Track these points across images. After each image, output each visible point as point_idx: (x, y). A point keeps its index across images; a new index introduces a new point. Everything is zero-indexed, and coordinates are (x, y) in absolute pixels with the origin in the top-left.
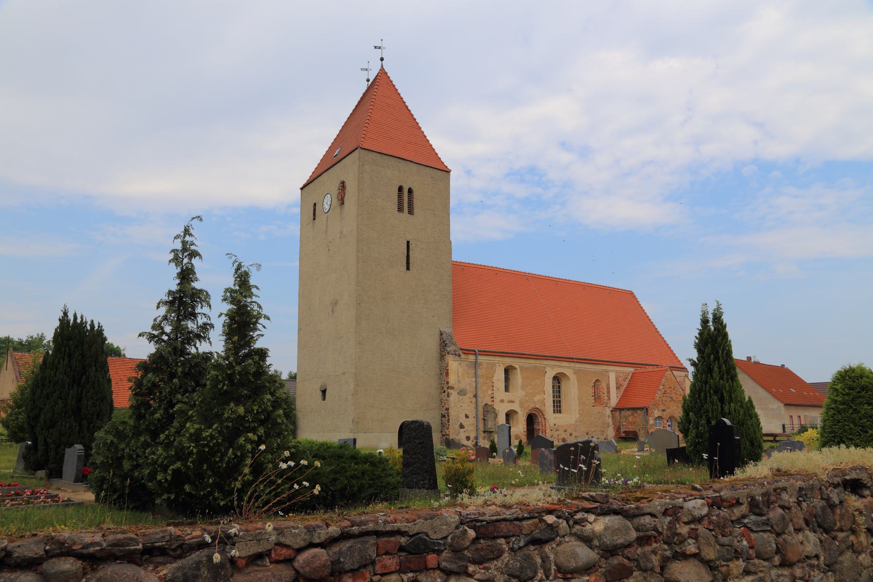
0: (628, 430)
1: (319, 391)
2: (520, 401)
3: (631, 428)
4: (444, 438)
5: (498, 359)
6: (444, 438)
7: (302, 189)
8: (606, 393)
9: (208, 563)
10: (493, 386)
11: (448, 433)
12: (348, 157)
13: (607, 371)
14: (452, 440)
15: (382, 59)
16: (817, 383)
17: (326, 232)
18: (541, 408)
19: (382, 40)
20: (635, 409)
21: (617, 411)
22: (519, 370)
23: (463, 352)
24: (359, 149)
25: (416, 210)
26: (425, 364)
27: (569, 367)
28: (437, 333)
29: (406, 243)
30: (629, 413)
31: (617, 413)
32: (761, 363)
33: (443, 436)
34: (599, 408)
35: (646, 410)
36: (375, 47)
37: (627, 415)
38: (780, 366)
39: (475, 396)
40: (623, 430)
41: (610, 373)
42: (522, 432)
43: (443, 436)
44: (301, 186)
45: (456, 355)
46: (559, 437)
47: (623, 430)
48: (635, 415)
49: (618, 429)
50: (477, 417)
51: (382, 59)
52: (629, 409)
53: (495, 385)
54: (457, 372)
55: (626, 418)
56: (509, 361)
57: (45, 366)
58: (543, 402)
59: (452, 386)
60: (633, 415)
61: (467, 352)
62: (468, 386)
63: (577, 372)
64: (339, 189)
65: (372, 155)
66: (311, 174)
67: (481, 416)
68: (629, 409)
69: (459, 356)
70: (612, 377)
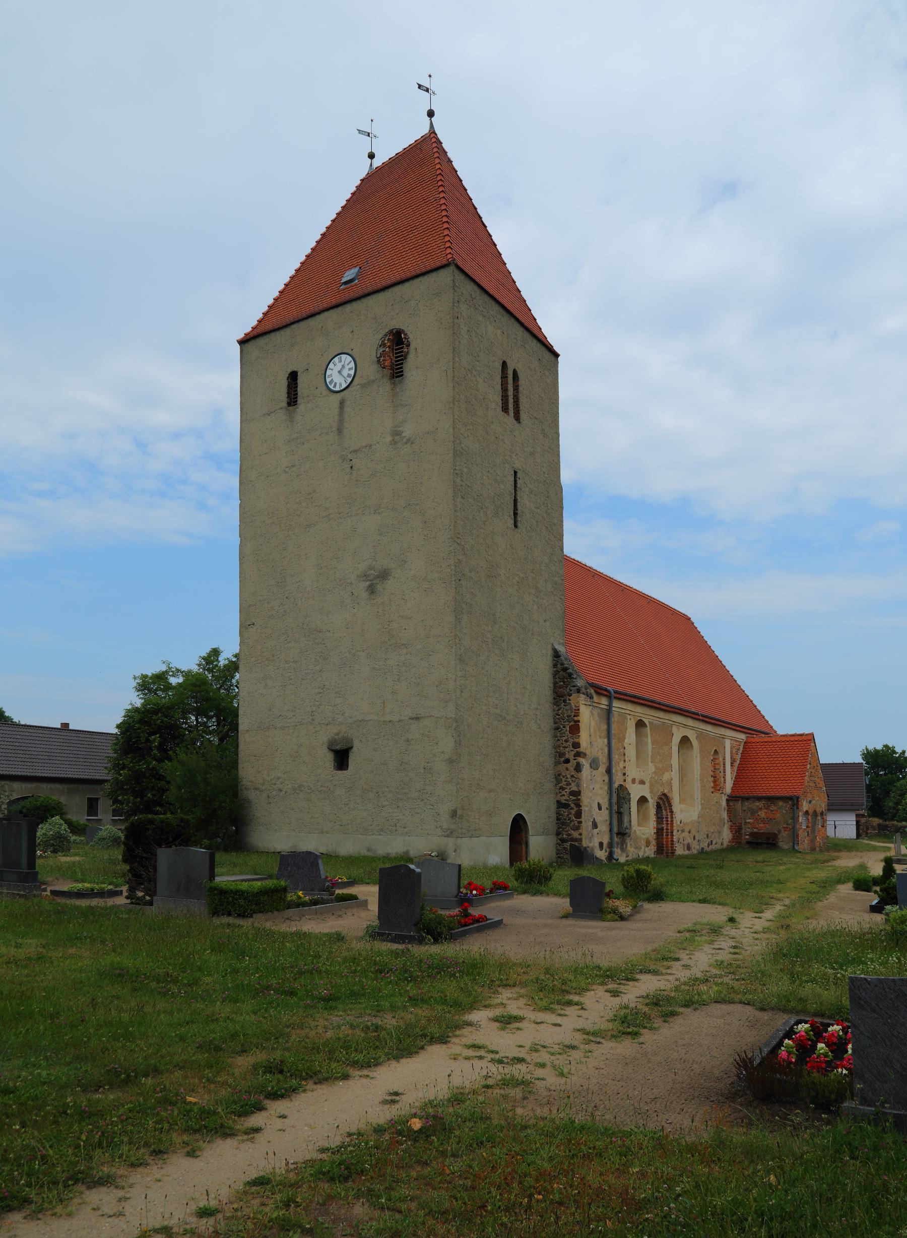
0: (755, 830)
1: (326, 750)
2: (650, 782)
3: (762, 828)
4: (567, 845)
5: (630, 707)
6: (567, 845)
7: (242, 342)
8: (722, 772)
9: (332, 1175)
10: (624, 755)
11: (575, 834)
12: (416, 282)
13: (723, 737)
14: (585, 848)
15: (431, 114)
16: (836, 764)
17: (340, 431)
18: (668, 795)
19: (430, 76)
20: (772, 799)
21: (738, 801)
22: (648, 728)
23: (596, 692)
24: (452, 267)
25: (523, 416)
26: (537, 709)
27: (693, 728)
28: (550, 653)
29: (513, 473)
30: (760, 804)
31: (739, 805)
32: (22, 723)
33: (563, 841)
34: (717, 795)
35: (794, 801)
36: (420, 86)
37: (755, 808)
38: (59, 727)
39: (609, 771)
40: (746, 830)
41: (726, 740)
42: (653, 833)
43: (563, 841)
44: (241, 336)
45: (588, 696)
46: (685, 842)
47: (746, 830)
48: (773, 808)
49: (737, 831)
50: (610, 808)
51: (431, 114)
52: (759, 799)
53: (626, 751)
54: (588, 727)
55: (753, 812)
56: (641, 712)
57: (458, 617)
58: (670, 783)
59: (584, 751)
60: (767, 808)
61: (600, 691)
62: (600, 752)
63: (701, 736)
64: (383, 345)
65: (471, 287)
66: (255, 323)
67: (615, 808)
68: (759, 799)
69: (592, 698)
70: (728, 744)
